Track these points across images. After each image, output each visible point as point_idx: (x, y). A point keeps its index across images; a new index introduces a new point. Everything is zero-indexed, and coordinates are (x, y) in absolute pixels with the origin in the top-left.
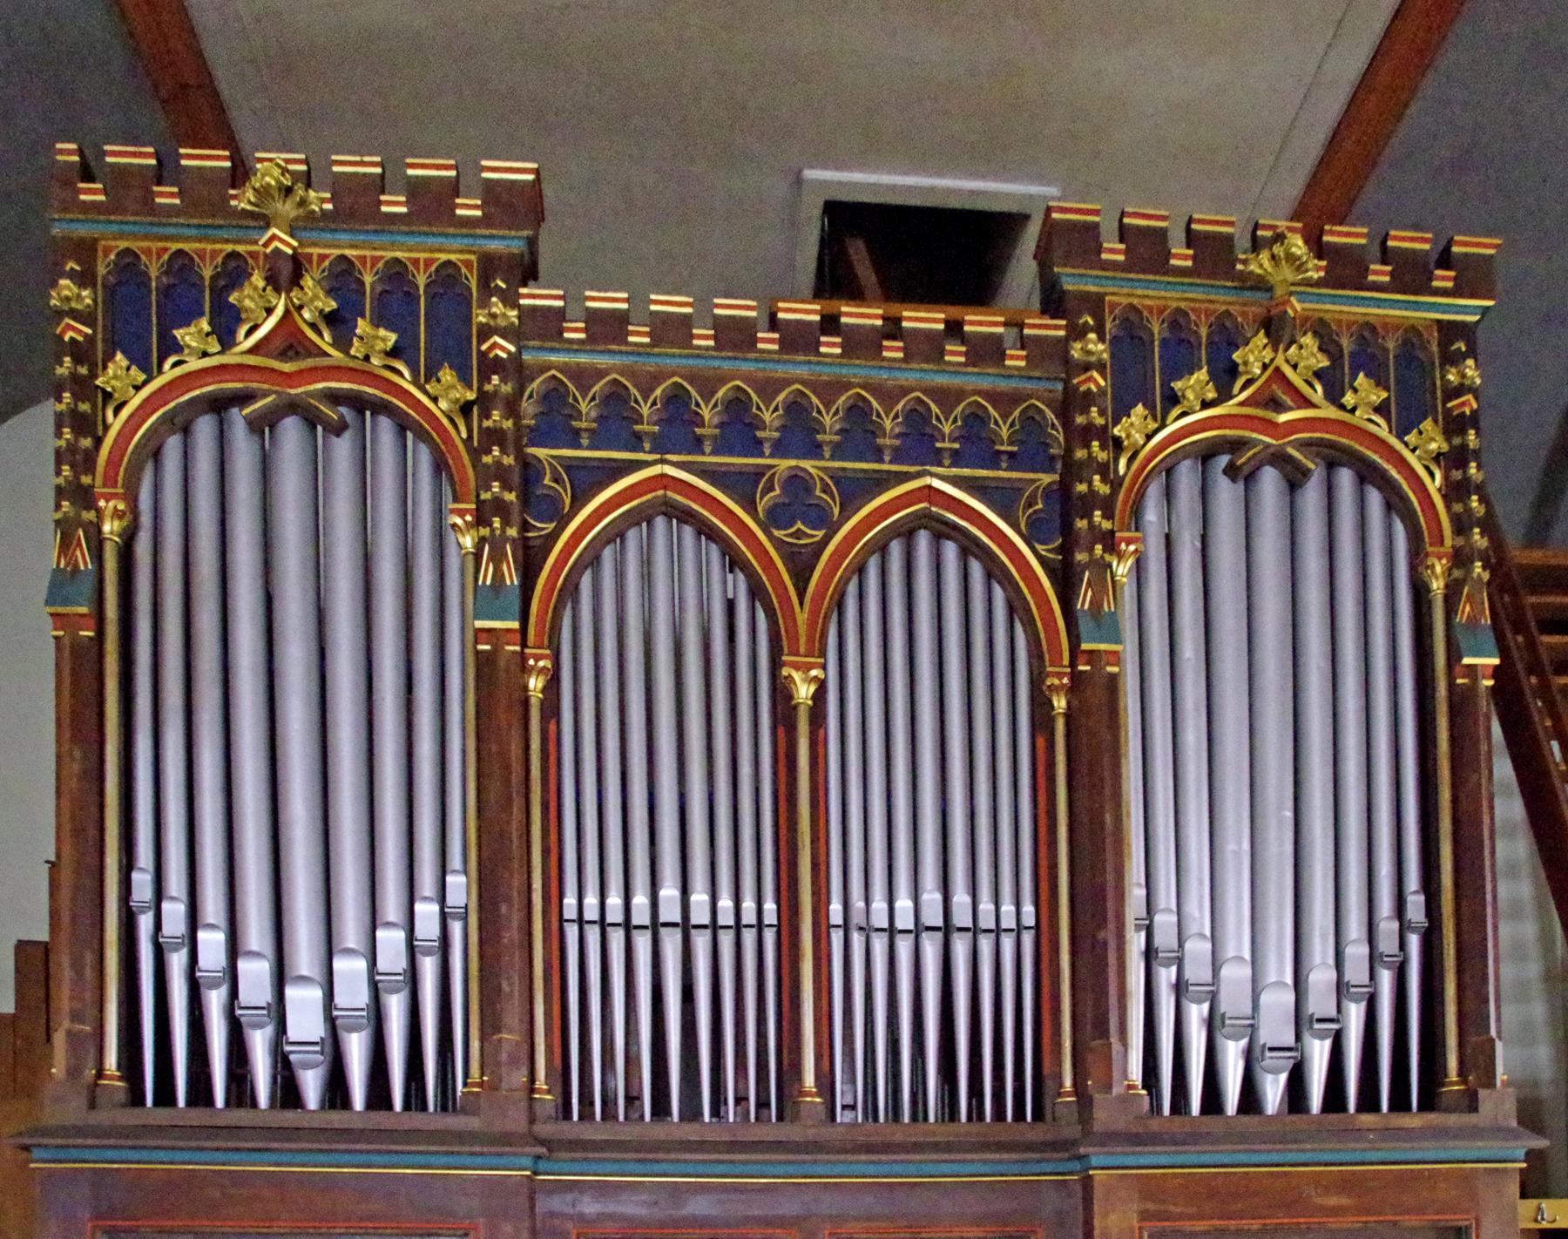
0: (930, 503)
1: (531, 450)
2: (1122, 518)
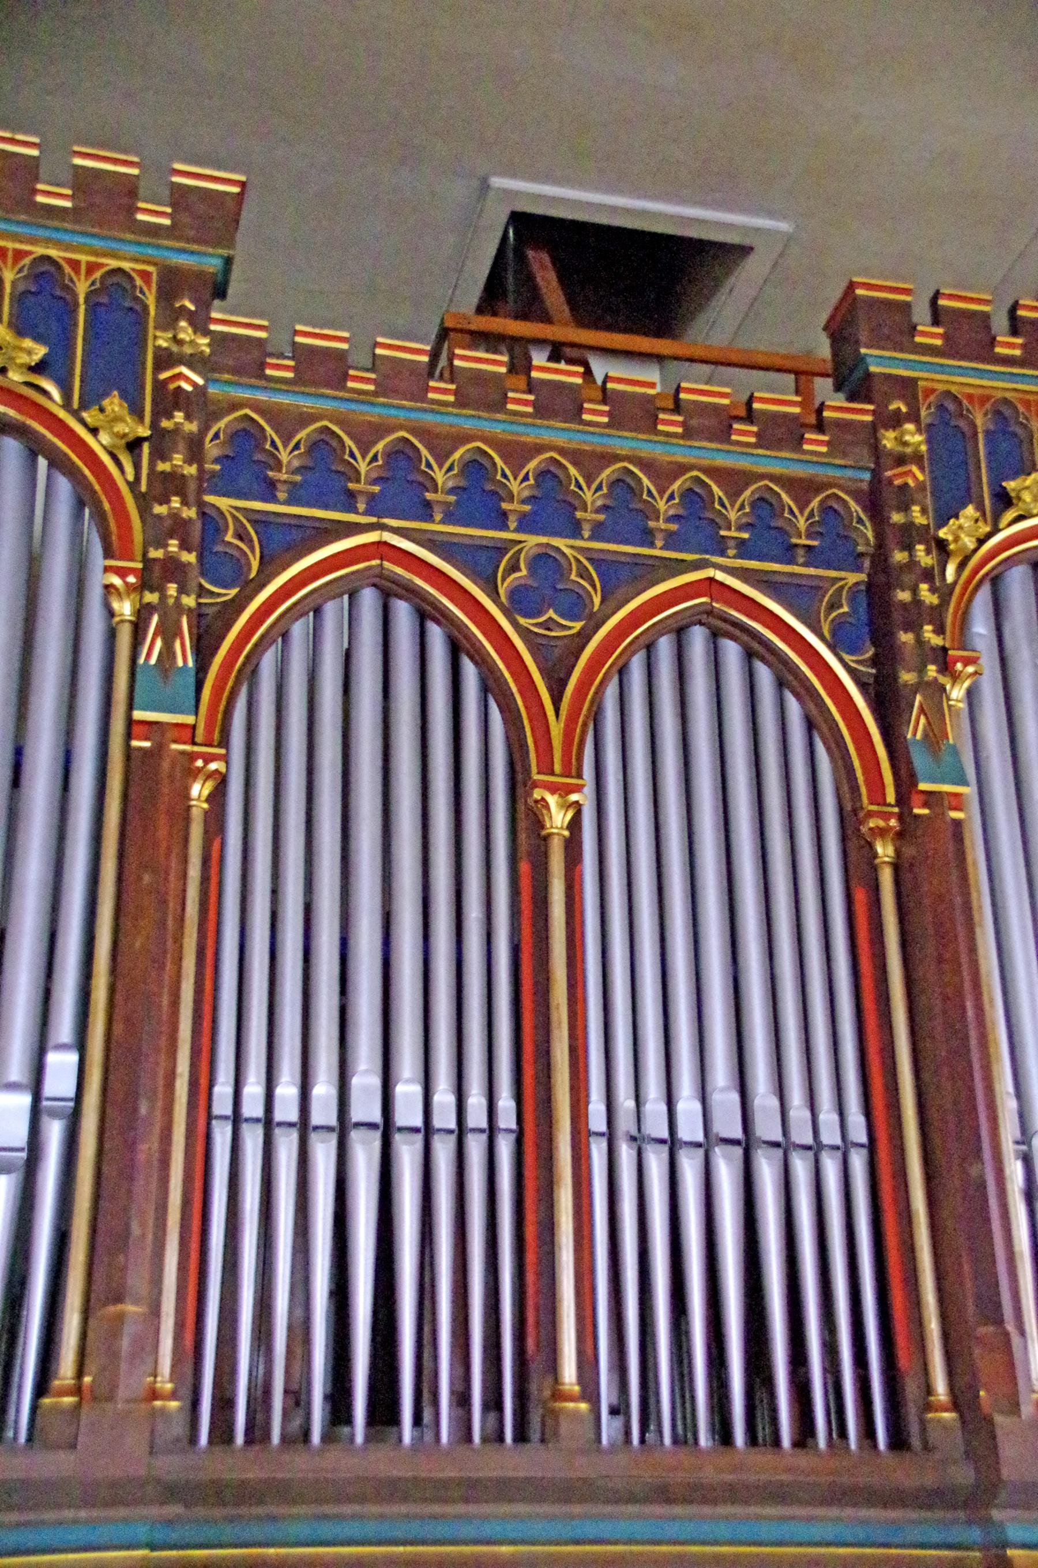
0: (382, 559)
1: (210, 499)
2: (953, 633)
